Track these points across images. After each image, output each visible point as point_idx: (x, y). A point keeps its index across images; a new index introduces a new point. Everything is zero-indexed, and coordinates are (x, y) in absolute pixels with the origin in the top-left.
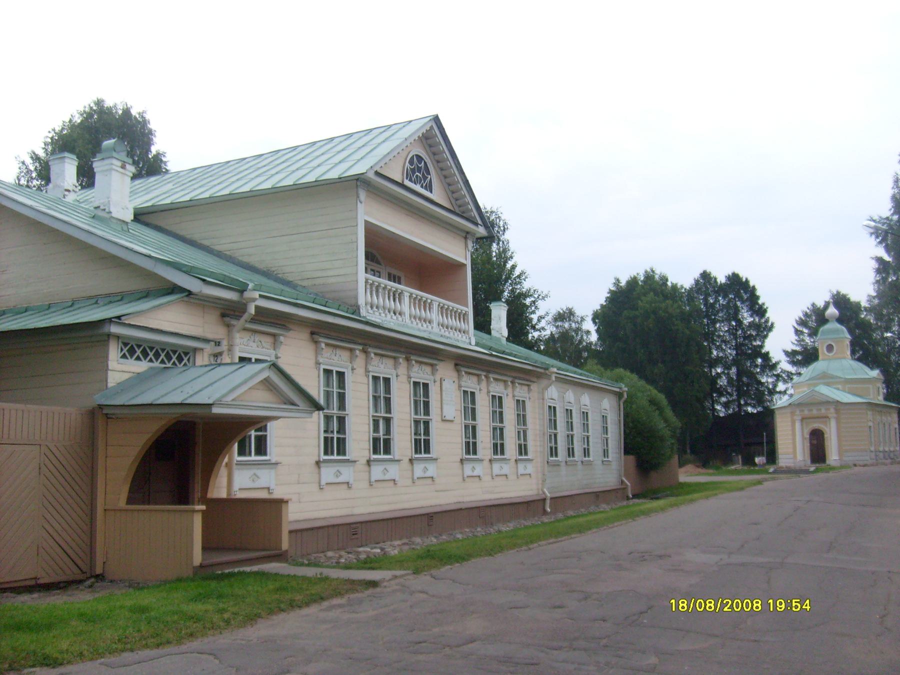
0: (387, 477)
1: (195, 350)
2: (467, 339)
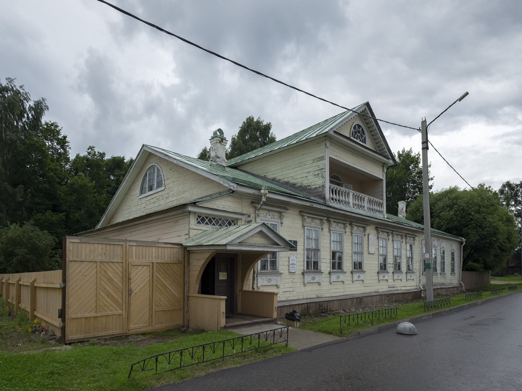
0: (360, 279)
1: (237, 219)
2: (383, 215)
